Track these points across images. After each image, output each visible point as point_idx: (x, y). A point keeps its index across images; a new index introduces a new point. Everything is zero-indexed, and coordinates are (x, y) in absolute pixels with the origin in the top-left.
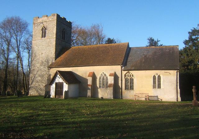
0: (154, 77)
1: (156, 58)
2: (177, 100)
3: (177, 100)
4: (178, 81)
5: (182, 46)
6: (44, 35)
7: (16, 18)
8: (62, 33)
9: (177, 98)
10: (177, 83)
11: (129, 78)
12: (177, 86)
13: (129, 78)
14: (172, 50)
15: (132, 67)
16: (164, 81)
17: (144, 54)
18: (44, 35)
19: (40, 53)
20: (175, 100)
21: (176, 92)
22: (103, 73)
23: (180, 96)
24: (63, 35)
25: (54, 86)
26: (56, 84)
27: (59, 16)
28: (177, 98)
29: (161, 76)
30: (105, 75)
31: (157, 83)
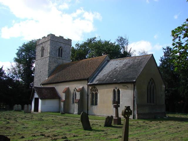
0: (114, 91)
22: (76, 88)
29: (120, 89)
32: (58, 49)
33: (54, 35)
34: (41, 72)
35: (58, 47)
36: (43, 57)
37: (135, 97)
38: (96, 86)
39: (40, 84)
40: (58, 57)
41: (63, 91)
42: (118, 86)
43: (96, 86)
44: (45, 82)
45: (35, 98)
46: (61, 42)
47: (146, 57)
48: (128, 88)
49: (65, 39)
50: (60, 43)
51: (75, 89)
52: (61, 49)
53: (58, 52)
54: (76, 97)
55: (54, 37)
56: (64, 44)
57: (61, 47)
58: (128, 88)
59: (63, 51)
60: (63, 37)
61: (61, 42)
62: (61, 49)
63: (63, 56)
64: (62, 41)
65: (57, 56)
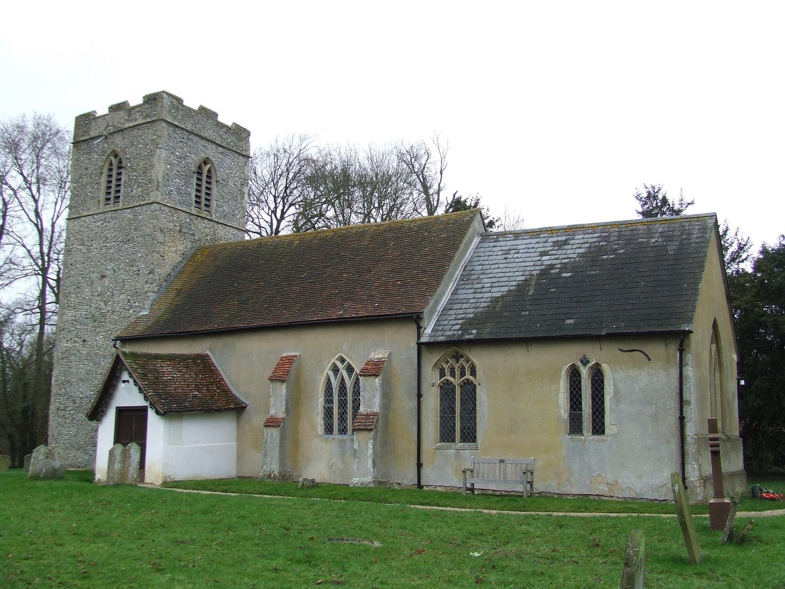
0: (574, 375)
13: (456, 381)
16: (616, 392)
22: (343, 360)
26: (120, 411)
29: (605, 367)
30: (350, 369)
31: (587, 411)
32: (194, 168)
33: (180, 101)
34: (103, 277)
35: (194, 160)
36: (121, 206)
37: (689, 403)
38: (460, 351)
39: (115, 340)
40: (194, 211)
41: (269, 373)
42: (596, 353)
43: (460, 351)
44: (140, 329)
45: (120, 411)
46: (206, 139)
47: (263, 202)
48: (649, 360)
49: (224, 126)
50: (204, 142)
51: (339, 364)
52: (206, 169)
53: (195, 187)
54: (356, 407)
55: (177, 110)
56: (221, 149)
57: (205, 163)
58: (649, 360)
59: (213, 181)
60: (216, 115)
61: (206, 139)
62: (206, 169)
63: (214, 204)
64: (209, 133)
65: (189, 205)
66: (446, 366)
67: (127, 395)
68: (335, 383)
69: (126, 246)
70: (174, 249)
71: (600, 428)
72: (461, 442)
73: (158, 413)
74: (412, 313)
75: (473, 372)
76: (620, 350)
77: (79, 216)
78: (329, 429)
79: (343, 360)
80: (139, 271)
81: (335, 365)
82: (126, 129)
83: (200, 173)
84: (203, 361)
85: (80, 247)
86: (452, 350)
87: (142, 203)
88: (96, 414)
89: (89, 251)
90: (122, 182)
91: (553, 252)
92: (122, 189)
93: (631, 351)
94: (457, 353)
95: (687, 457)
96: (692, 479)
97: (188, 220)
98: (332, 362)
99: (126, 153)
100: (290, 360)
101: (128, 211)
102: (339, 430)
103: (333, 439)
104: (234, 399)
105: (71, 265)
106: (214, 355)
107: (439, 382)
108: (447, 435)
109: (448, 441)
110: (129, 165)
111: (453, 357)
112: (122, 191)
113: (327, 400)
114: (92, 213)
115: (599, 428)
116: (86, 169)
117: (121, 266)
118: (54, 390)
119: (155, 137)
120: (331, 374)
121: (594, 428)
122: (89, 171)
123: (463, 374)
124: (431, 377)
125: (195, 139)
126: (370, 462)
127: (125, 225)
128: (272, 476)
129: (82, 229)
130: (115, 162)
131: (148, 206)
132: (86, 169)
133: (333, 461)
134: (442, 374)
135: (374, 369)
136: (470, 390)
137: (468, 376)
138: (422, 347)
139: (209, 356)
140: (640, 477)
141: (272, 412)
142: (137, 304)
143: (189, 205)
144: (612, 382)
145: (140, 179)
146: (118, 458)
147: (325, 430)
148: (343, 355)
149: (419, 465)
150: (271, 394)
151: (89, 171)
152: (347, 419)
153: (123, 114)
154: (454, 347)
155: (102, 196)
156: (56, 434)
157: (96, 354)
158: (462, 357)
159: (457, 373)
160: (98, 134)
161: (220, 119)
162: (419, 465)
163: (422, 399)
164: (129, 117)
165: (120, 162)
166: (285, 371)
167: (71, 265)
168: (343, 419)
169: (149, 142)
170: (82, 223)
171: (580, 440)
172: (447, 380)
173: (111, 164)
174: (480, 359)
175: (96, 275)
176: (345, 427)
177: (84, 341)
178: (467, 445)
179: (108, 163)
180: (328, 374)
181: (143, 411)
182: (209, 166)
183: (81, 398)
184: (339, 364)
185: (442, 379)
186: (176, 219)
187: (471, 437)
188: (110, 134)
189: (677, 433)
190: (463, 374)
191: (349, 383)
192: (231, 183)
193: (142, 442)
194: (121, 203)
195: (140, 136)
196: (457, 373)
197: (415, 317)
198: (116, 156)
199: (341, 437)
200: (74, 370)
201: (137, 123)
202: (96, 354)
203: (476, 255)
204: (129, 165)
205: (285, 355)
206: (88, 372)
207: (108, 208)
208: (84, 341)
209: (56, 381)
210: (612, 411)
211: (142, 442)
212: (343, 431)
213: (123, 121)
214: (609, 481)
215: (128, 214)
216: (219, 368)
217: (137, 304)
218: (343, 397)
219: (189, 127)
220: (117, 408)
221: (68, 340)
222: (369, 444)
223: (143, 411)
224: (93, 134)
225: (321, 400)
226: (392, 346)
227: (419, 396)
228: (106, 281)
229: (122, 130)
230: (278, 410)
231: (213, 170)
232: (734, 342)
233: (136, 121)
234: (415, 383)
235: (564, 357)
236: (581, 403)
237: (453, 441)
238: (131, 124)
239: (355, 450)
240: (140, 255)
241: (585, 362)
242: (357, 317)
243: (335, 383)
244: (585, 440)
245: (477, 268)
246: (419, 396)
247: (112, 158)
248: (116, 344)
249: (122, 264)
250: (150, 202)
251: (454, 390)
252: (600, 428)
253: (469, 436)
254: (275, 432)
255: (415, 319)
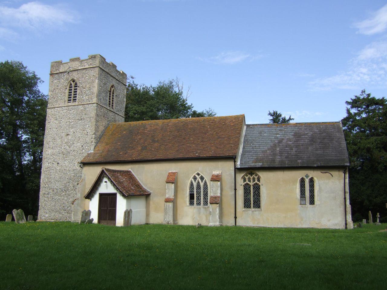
0: (302, 181)
1: (299, 151)
2: (346, 228)
3: (346, 228)
4: (347, 190)
5: (376, 99)
6: (72, 96)
7: (143, 88)
8: (108, 94)
9: (346, 224)
10: (345, 192)
11: (251, 184)
12: (345, 198)
13: (251, 184)
14: (320, 132)
15: (257, 161)
16: (320, 189)
17: (277, 138)
18: (72, 96)
19: (63, 135)
20: (342, 227)
21: (344, 212)
22: (198, 174)
23: (350, 204)
24: (110, 99)
25: (96, 200)
26: (101, 195)
27: (105, 59)
28: (346, 224)
29: (315, 178)
30: (202, 178)
31: (308, 194)
36: (77, 103)
41: (165, 179)
42: (311, 174)
45: (101, 195)
48: (332, 176)
50: (112, 78)
51: (197, 176)
54: (206, 194)
56: (117, 81)
58: (332, 176)
63: (114, 105)
66: (247, 178)
67: (106, 188)
68: (195, 184)
69: (80, 122)
70: (102, 124)
71: (313, 202)
72: (253, 208)
73: (124, 196)
74: (233, 156)
75: (259, 180)
76: (321, 172)
77: (54, 107)
78: (192, 203)
79: (198, 174)
80: (87, 133)
81: (195, 176)
82: (80, 70)
83: (110, 91)
84: (128, 173)
85: (55, 121)
86: (249, 171)
87: (89, 103)
88: (89, 196)
89: (60, 123)
90: (78, 93)
91: (281, 134)
92: (77, 96)
93: (326, 173)
94: (251, 172)
95: (347, 213)
96: (349, 221)
97: (106, 111)
98: (194, 175)
99: (79, 80)
100: (174, 174)
101: (81, 106)
102: (197, 204)
103: (195, 207)
104: (145, 191)
105: (50, 129)
106: (133, 171)
107: (243, 184)
108: (247, 205)
109: (248, 208)
110: (81, 86)
111: (249, 174)
112: (77, 97)
113: (191, 191)
114: (61, 106)
115: (312, 202)
116: (58, 86)
117: (77, 131)
118: (42, 185)
119: (95, 74)
120: (193, 180)
121: (310, 202)
122: (59, 87)
123: (254, 180)
124: (240, 182)
125: (109, 76)
126: (218, 216)
127: (79, 112)
128: (170, 223)
129: (56, 113)
130: (73, 84)
131: (92, 104)
132: (58, 86)
133: (195, 216)
134: (245, 180)
135: (216, 179)
136: (257, 188)
137: (256, 181)
138: (238, 170)
139: (131, 172)
140: (329, 221)
141: (167, 196)
142: (86, 148)
143: (107, 105)
144: (318, 184)
145: (87, 92)
146: (127, 214)
147: (190, 204)
148: (199, 172)
149: (236, 218)
150: (167, 188)
151: (59, 87)
152: (201, 199)
153: (78, 63)
154: (250, 170)
155: (67, 99)
156: (43, 205)
157: (65, 169)
158: (253, 174)
159: (252, 181)
160: (64, 71)
161: (118, 69)
162: (236, 218)
163: (236, 191)
164: (81, 64)
165: (76, 84)
166: (172, 179)
167: (50, 129)
168: (199, 199)
169: (92, 76)
170: (56, 110)
171: (305, 207)
172: (247, 183)
173: (71, 85)
174: (264, 176)
175: (63, 134)
176: (200, 202)
177: (58, 163)
178: (257, 209)
179: (69, 84)
180: (191, 180)
181: (115, 195)
182: (113, 88)
183: (57, 189)
184: (197, 176)
185: (245, 183)
186: (102, 111)
187: (258, 206)
188: (71, 71)
189: (344, 204)
190: (254, 180)
191: (202, 184)
192: (120, 97)
193: (114, 208)
194: (77, 102)
195: (87, 73)
196: (252, 181)
197: (234, 157)
198: (74, 81)
199: (199, 206)
200: (53, 176)
201: (85, 67)
202: (65, 169)
203: (247, 133)
204: (81, 86)
205: (170, 172)
206: (60, 178)
207: (70, 104)
208: (58, 163)
209: (43, 181)
210: (318, 195)
211: (114, 208)
212: (199, 204)
213: (77, 66)
214: (317, 222)
215: (81, 107)
216: (136, 177)
217: (86, 148)
218: (199, 190)
219: (107, 71)
220: (99, 193)
221: (49, 163)
222: (217, 209)
223: (115, 195)
224: (61, 71)
225: (188, 191)
226: (225, 169)
227: (235, 189)
228: (70, 137)
229: (77, 70)
230: (170, 194)
231: (115, 91)
232: (92, 186)
233: (85, 66)
234: (233, 185)
235: (299, 174)
236: (305, 193)
237: (250, 207)
238: (82, 68)
239: (210, 212)
240: (88, 126)
241: (307, 176)
242: (207, 157)
243: (195, 184)
244: (307, 207)
245: (249, 138)
246: (235, 189)
247: (72, 82)
248: (81, 165)
249: (78, 130)
250: (93, 103)
251: (250, 187)
252: (313, 202)
253: (257, 205)
254: (171, 205)
255: (233, 158)
